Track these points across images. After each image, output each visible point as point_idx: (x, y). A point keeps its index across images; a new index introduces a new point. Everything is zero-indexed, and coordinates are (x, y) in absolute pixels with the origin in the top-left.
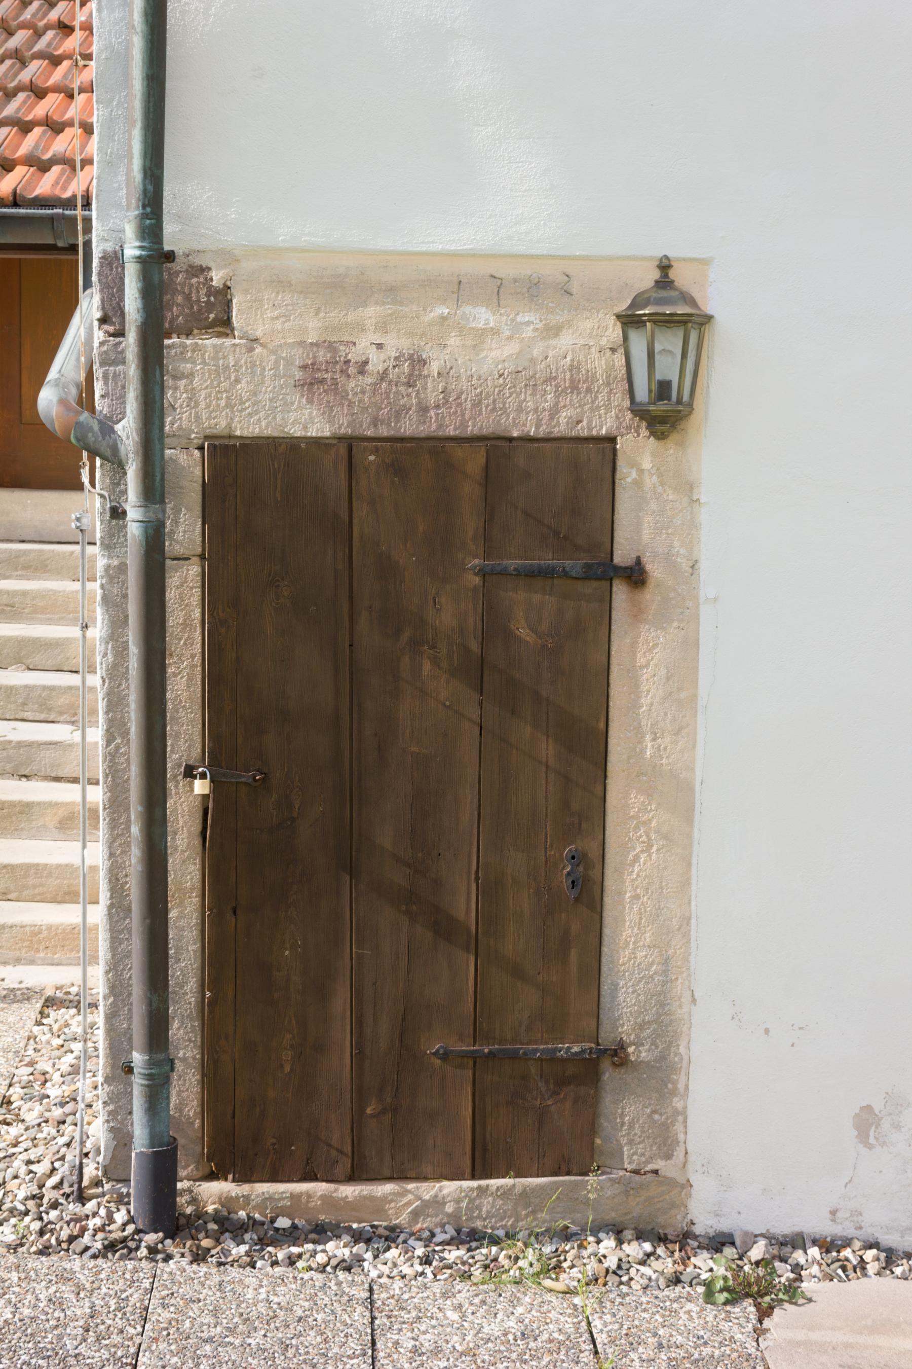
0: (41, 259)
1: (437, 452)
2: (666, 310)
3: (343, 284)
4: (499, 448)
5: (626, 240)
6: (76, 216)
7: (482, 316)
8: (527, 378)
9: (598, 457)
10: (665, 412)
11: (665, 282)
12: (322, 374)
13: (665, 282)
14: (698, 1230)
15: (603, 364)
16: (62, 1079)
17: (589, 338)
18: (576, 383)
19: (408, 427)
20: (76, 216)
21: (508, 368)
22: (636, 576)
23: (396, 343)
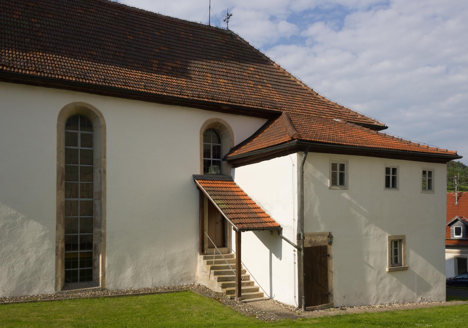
0: (73, 146)
1: (317, 247)
2: (330, 236)
3: (311, 235)
4: (320, 246)
5: (328, 231)
6: (81, 249)
7: (319, 237)
8: (322, 241)
9: (326, 247)
10: (330, 243)
11: (330, 234)
12: (310, 242)
13: (330, 234)
14: (226, 162)
15: (327, 240)
16: (226, 22)
17: (326, 238)
18: (325, 241)
19: (315, 246)
20: (78, 250)
21: (321, 241)
22: (329, 256)
23: (315, 239)
